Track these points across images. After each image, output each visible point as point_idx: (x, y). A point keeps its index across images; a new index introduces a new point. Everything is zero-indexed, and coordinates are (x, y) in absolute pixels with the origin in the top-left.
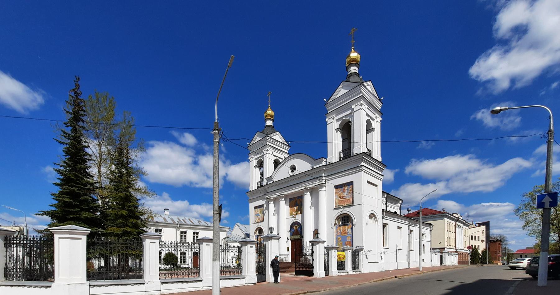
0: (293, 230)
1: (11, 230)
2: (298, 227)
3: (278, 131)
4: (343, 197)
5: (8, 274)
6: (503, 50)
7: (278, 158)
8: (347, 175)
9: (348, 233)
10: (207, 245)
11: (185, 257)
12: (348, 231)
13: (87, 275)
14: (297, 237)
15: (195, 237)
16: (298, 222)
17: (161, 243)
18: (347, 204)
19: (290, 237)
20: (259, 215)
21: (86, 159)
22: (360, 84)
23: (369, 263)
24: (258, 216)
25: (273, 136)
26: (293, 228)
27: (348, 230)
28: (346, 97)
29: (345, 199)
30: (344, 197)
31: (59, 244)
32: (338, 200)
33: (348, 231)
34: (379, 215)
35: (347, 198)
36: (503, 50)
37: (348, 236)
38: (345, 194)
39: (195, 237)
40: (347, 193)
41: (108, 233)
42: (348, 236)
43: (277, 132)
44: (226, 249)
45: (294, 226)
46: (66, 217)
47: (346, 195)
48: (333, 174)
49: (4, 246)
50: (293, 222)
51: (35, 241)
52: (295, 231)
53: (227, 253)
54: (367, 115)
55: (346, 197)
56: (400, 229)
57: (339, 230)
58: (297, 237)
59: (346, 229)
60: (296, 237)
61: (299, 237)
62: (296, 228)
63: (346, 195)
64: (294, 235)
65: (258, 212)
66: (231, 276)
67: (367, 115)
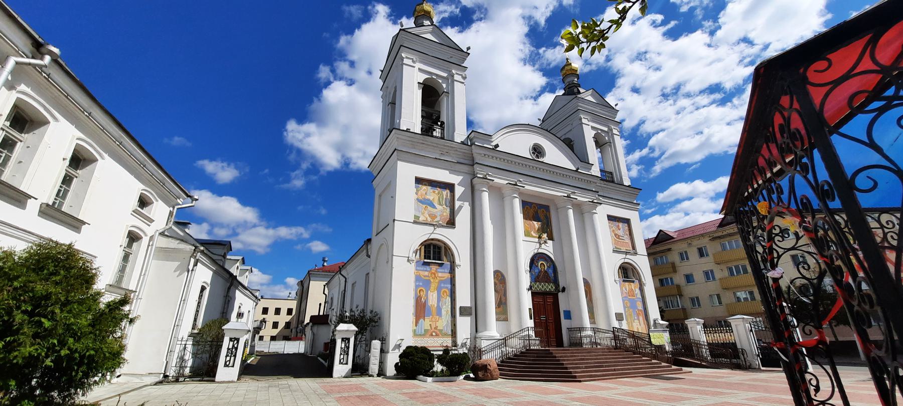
0: (537, 271)
2: (548, 267)
6: (833, 284)
8: (619, 207)
10: (320, 304)
14: (543, 287)
18: (626, 250)
21: (845, 232)
25: (586, 97)
26: (537, 266)
28: (605, 111)
29: (620, 240)
30: (621, 237)
31: (438, 58)
36: (833, 284)
38: (620, 233)
44: (723, 330)
48: (605, 197)
50: (536, 251)
51: (38, 375)
52: (540, 272)
53: (709, 334)
54: (593, 128)
56: (441, 266)
57: (624, 288)
61: (552, 287)
64: (540, 282)
67: (593, 128)
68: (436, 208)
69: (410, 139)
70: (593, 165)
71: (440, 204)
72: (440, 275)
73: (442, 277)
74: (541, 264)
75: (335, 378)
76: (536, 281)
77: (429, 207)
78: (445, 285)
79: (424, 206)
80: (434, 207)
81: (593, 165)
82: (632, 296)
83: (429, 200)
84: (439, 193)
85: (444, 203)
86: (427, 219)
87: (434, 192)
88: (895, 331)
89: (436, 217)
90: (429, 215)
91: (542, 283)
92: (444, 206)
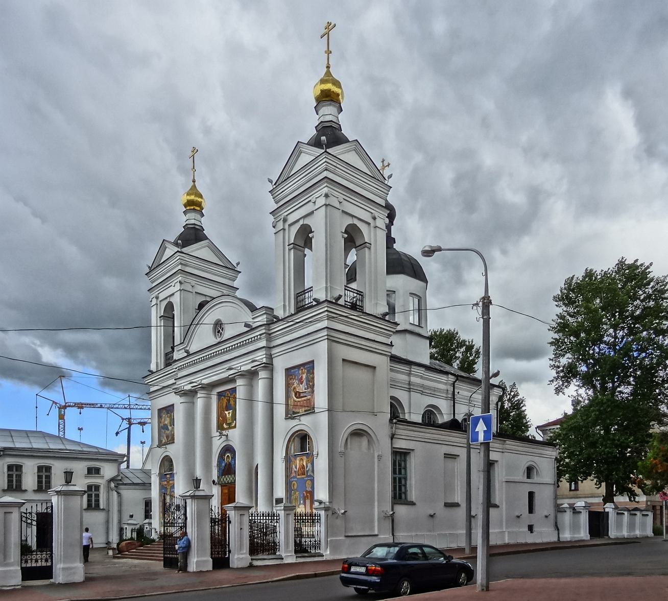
0: (223, 465)
1: (531, 539)
4: (300, 393)
7: (301, 222)
9: (307, 471)
11: (48, 478)
15: (44, 476)
16: (235, 451)
17: (278, 518)
19: (218, 477)
20: (168, 429)
23: (348, 540)
27: (307, 467)
30: (302, 395)
32: (292, 400)
34: (380, 425)
35: (306, 396)
39: (44, 476)
41: (573, 427)
47: (305, 389)
49: (491, 298)
55: (305, 395)
59: (305, 464)
63: (305, 389)
64: (225, 475)
65: (166, 422)
66: (108, 504)
71: (171, 426)
80: (168, 430)
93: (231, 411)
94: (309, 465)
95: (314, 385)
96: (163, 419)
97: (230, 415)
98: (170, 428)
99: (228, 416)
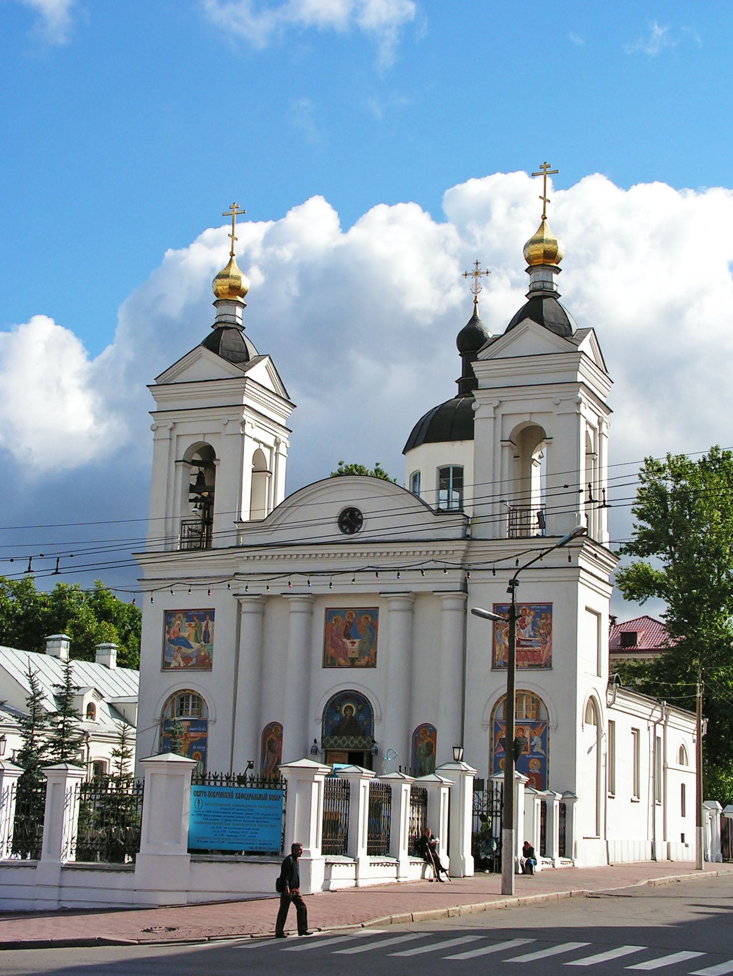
0: (337, 719)
2: (359, 711)
3: (527, 317)
5: (625, 598)
9: (533, 747)
12: (533, 743)
13: (435, 442)
22: (285, 397)
24: (184, 649)
26: (339, 711)
27: (532, 740)
32: (503, 647)
33: (533, 743)
37: (532, 758)
40: (532, 633)
42: (532, 758)
43: (525, 318)
45: (341, 706)
46: (35, 790)
58: (352, 742)
60: (332, 742)
62: (348, 712)
65: (185, 634)
68: (192, 648)
69: (147, 544)
70: (612, 412)
71: (197, 641)
72: (192, 734)
73: (193, 737)
74: (346, 708)
75: (496, 339)
76: (333, 734)
77: (182, 647)
78: (198, 748)
79: (177, 647)
80: (190, 647)
81: (612, 412)
82: (335, 838)
83: (183, 638)
84: (196, 625)
85: (202, 639)
86: (180, 664)
87: (190, 625)
88: (642, 950)
89: (190, 659)
90: (183, 658)
91: (344, 737)
92: (203, 643)
93: (357, 641)
94: (537, 739)
95: (549, 633)
96: (175, 628)
97: (356, 645)
98: (196, 645)
99: (349, 646)
